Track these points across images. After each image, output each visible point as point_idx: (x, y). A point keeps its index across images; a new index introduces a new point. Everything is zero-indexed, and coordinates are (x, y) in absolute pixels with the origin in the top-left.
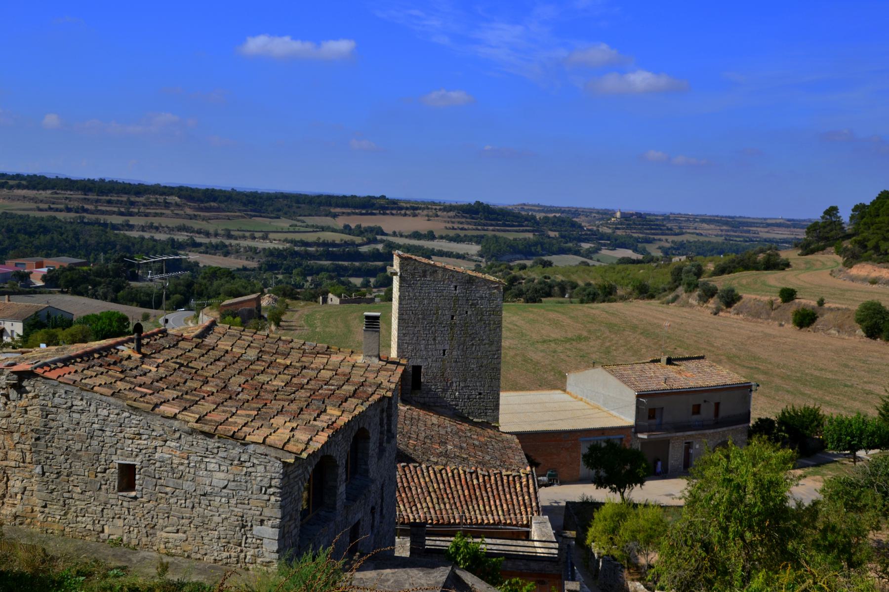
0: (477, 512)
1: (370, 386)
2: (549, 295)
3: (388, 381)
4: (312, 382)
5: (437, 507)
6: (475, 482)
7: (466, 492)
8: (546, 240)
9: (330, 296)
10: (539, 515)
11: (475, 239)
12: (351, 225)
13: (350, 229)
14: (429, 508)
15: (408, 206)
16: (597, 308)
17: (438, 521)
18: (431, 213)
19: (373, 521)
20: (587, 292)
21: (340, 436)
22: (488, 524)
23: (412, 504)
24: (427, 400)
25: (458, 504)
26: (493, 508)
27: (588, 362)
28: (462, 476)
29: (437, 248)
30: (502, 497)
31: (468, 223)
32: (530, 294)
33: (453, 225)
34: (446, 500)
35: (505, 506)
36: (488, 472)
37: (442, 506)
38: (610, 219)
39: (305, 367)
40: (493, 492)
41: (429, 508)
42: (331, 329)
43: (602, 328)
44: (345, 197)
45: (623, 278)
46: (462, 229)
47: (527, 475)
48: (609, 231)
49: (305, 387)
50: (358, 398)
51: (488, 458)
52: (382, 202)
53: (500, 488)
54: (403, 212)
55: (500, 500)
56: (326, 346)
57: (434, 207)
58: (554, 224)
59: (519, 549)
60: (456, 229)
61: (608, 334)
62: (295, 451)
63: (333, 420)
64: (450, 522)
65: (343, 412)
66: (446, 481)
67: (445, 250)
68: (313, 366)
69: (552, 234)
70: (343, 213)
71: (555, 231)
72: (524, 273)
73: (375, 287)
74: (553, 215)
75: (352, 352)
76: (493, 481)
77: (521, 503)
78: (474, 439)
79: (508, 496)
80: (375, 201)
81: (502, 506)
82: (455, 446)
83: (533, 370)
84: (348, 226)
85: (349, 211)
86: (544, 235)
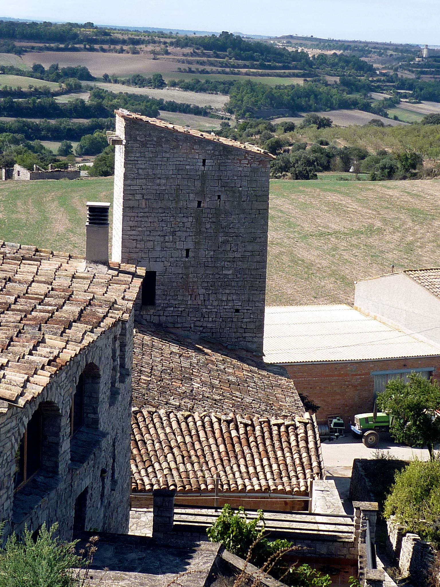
0: (237, 474)
1: (101, 306)
2: (327, 168)
3: (123, 298)
4: (22, 300)
5: (182, 468)
6: (234, 433)
7: (222, 448)
8: (323, 89)
9: (17, 167)
10: (321, 478)
11: (222, 86)
12: (43, 65)
13: (43, 71)
14: (170, 470)
15: (126, 37)
16: (395, 188)
17: (184, 487)
18: (158, 49)
19: (103, 488)
20: (381, 164)
21: (64, 375)
22: (253, 491)
23: (147, 464)
24: (163, 319)
25: (211, 464)
26: (259, 469)
27: (382, 264)
28: (216, 426)
29: (167, 99)
30: (271, 454)
31: (212, 64)
32: (300, 167)
33: (190, 66)
34: (194, 458)
35: (275, 467)
36: (251, 420)
37: (189, 466)
38: (414, 59)
39: (10, 280)
40: (257, 447)
41: (170, 470)
42: (19, 216)
43: (402, 217)
44: (34, 24)
45: (431, 145)
46: (203, 72)
47: (306, 424)
48: (413, 76)
49: (13, 307)
50: (86, 323)
51: (248, 399)
52: (89, 31)
53: (268, 442)
54: (118, 47)
55: (269, 459)
56: (33, 247)
57: (162, 40)
58: (333, 65)
59: (294, 525)
60: (193, 72)
61: (410, 224)
62: (7, 397)
63: (56, 353)
64: (199, 488)
65: (67, 342)
66: (193, 432)
67: (179, 102)
68: (17, 277)
69: (331, 80)
70: (33, 48)
71: (335, 75)
72: (291, 136)
73: (80, 155)
74: (333, 52)
75: (70, 257)
76: (258, 433)
77: (297, 462)
78: (229, 374)
79: (279, 453)
80: (75, 30)
81: (270, 466)
82: (203, 383)
83: (306, 275)
84: (40, 66)
85: (41, 45)
86: (319, 80)
